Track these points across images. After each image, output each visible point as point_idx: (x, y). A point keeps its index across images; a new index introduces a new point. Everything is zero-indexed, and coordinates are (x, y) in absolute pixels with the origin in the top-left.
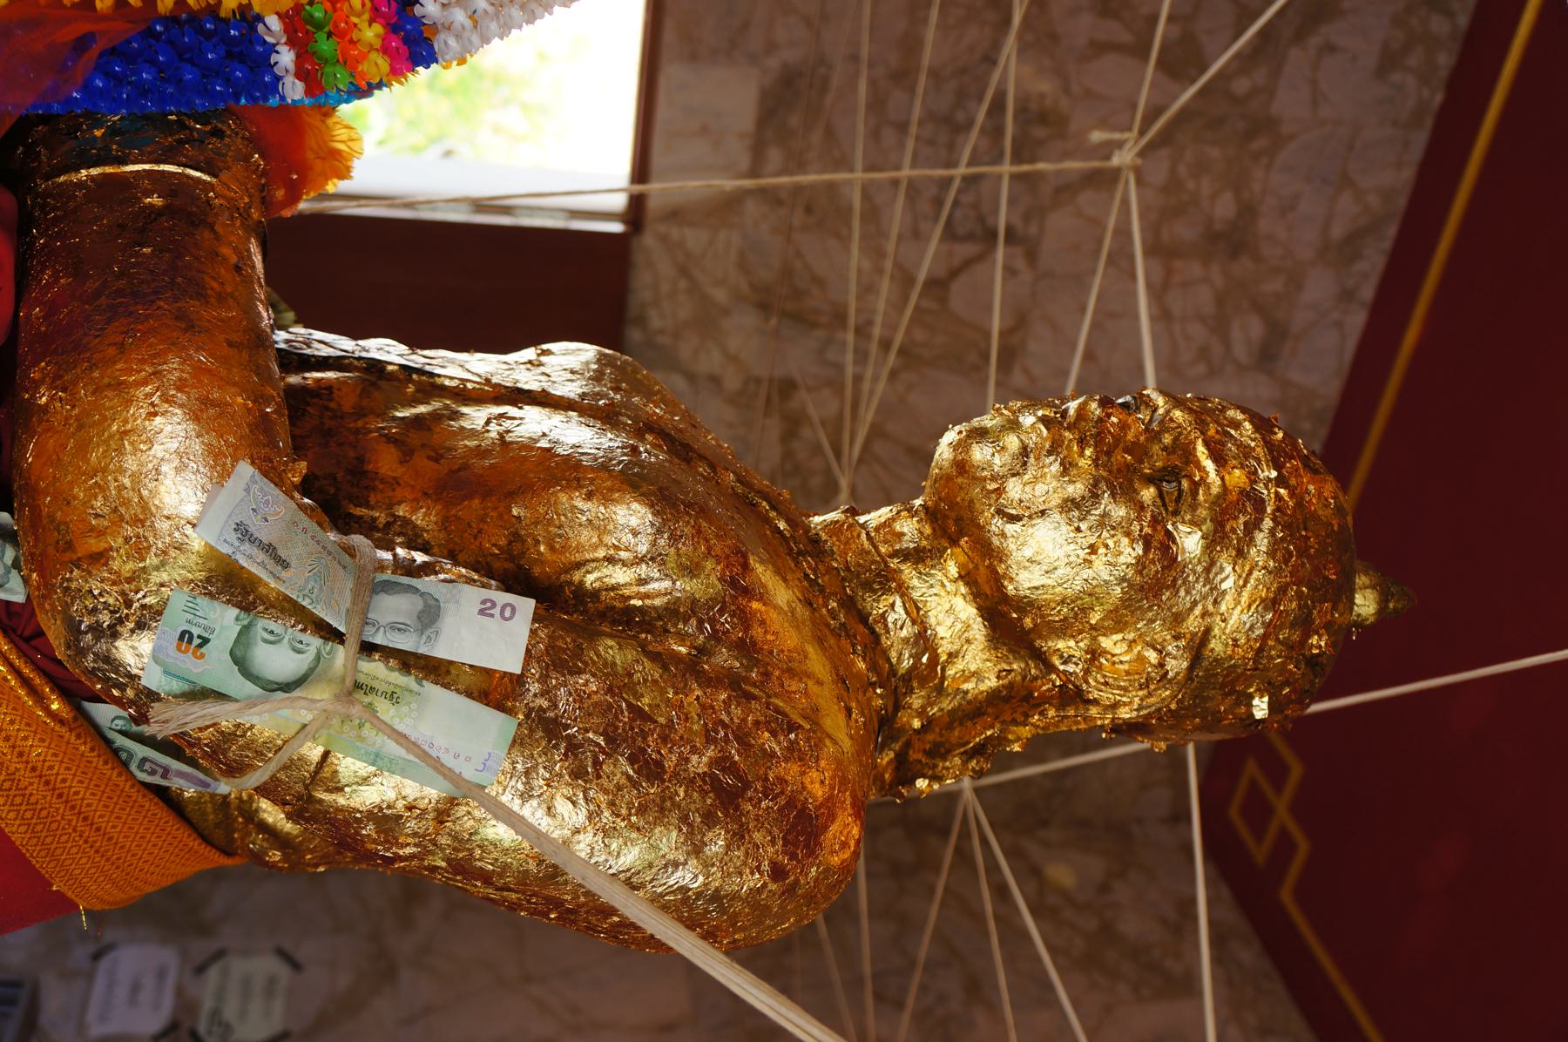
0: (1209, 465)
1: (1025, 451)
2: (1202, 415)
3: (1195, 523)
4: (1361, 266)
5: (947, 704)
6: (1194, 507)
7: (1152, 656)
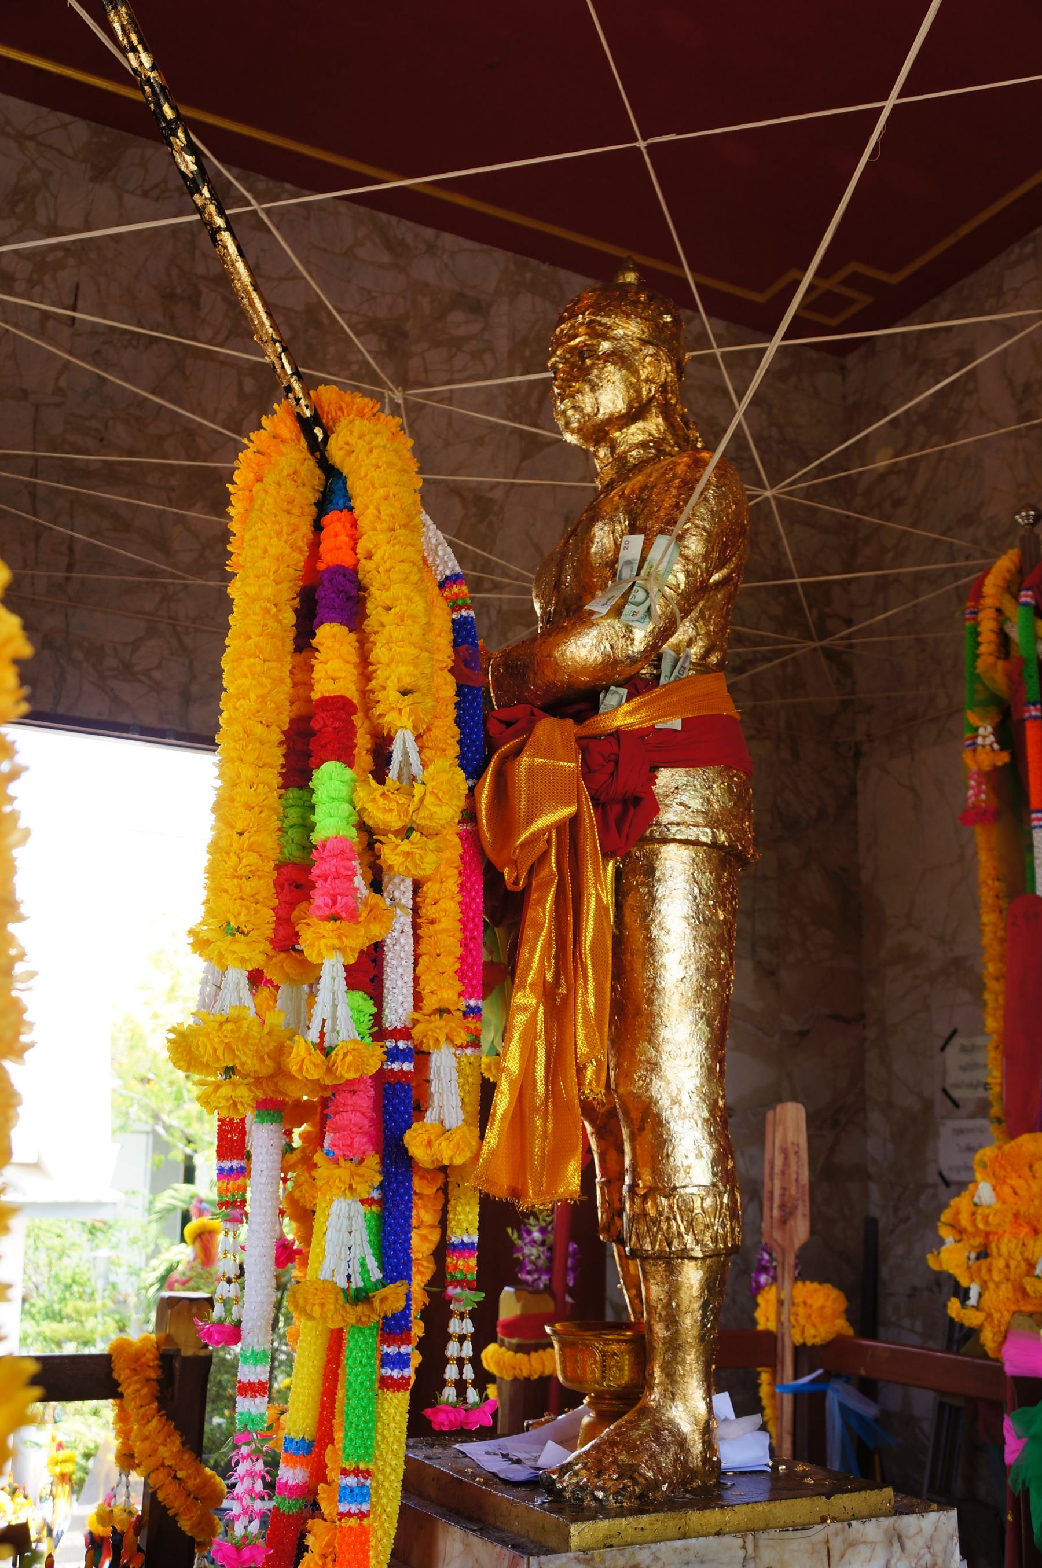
0: (578, 340)
1: (574, 407)
2: (559, 344)
3: (599, 344)
4: (410, 240)
5: (669, 437)
6: (592, 345)
7: (648, 359)
